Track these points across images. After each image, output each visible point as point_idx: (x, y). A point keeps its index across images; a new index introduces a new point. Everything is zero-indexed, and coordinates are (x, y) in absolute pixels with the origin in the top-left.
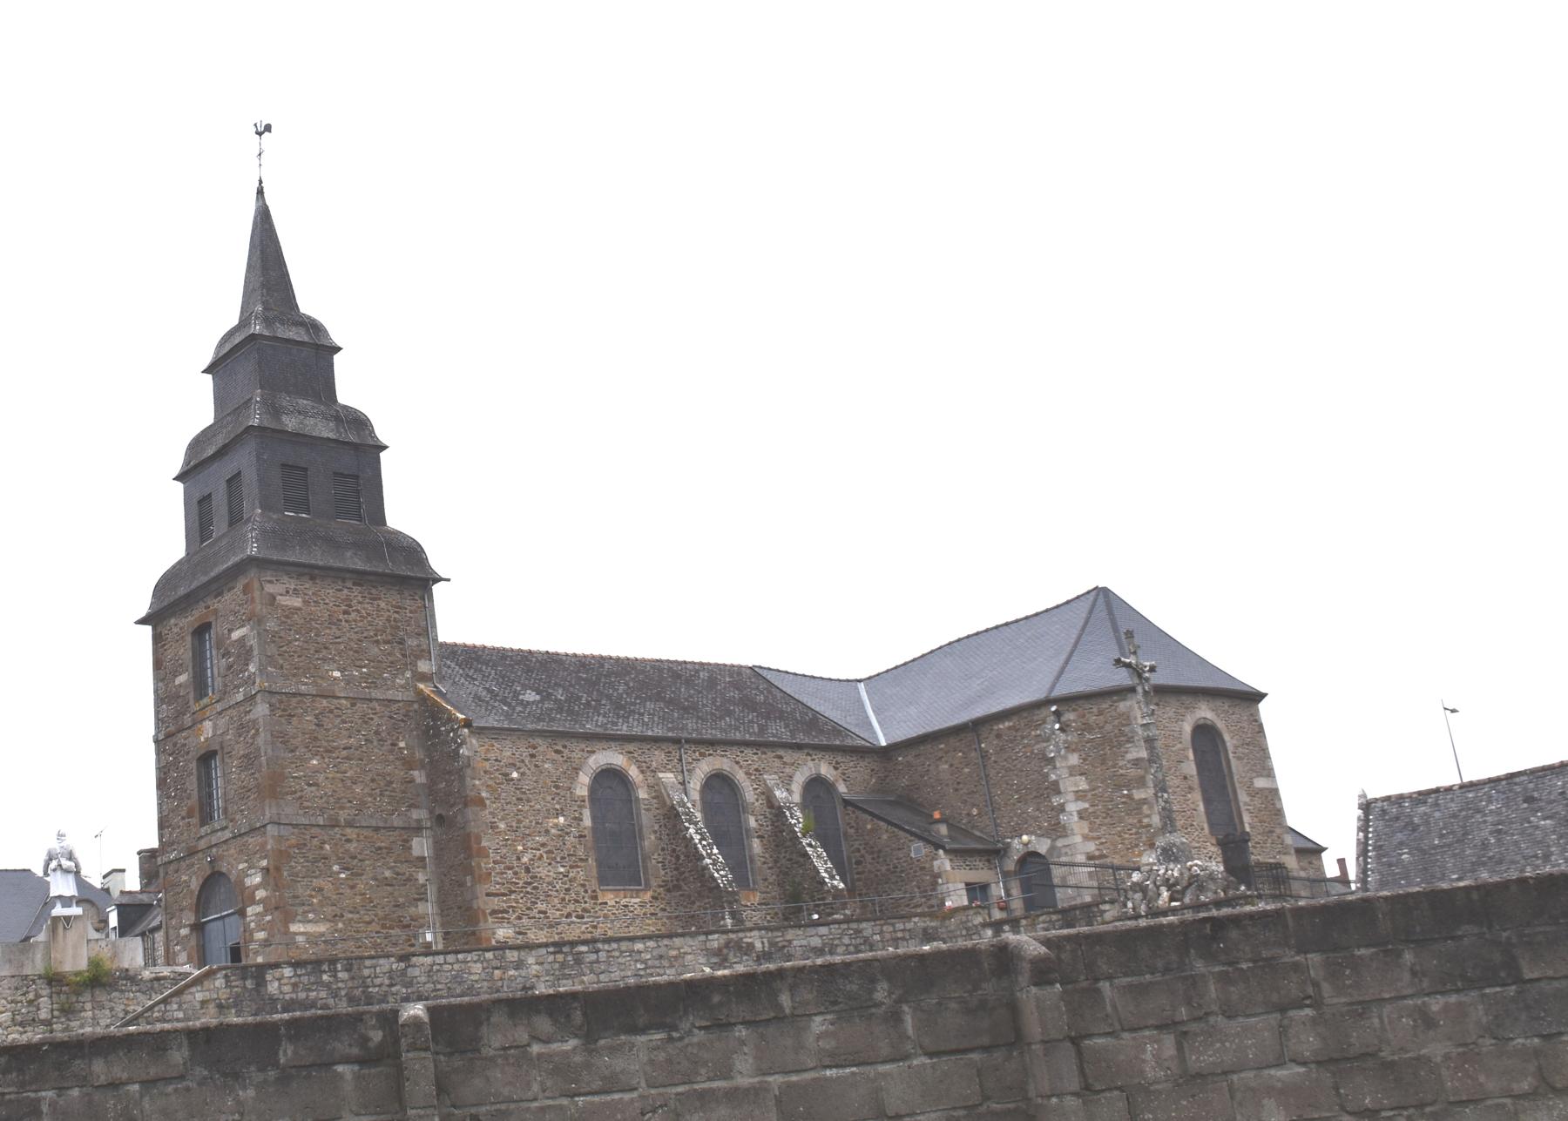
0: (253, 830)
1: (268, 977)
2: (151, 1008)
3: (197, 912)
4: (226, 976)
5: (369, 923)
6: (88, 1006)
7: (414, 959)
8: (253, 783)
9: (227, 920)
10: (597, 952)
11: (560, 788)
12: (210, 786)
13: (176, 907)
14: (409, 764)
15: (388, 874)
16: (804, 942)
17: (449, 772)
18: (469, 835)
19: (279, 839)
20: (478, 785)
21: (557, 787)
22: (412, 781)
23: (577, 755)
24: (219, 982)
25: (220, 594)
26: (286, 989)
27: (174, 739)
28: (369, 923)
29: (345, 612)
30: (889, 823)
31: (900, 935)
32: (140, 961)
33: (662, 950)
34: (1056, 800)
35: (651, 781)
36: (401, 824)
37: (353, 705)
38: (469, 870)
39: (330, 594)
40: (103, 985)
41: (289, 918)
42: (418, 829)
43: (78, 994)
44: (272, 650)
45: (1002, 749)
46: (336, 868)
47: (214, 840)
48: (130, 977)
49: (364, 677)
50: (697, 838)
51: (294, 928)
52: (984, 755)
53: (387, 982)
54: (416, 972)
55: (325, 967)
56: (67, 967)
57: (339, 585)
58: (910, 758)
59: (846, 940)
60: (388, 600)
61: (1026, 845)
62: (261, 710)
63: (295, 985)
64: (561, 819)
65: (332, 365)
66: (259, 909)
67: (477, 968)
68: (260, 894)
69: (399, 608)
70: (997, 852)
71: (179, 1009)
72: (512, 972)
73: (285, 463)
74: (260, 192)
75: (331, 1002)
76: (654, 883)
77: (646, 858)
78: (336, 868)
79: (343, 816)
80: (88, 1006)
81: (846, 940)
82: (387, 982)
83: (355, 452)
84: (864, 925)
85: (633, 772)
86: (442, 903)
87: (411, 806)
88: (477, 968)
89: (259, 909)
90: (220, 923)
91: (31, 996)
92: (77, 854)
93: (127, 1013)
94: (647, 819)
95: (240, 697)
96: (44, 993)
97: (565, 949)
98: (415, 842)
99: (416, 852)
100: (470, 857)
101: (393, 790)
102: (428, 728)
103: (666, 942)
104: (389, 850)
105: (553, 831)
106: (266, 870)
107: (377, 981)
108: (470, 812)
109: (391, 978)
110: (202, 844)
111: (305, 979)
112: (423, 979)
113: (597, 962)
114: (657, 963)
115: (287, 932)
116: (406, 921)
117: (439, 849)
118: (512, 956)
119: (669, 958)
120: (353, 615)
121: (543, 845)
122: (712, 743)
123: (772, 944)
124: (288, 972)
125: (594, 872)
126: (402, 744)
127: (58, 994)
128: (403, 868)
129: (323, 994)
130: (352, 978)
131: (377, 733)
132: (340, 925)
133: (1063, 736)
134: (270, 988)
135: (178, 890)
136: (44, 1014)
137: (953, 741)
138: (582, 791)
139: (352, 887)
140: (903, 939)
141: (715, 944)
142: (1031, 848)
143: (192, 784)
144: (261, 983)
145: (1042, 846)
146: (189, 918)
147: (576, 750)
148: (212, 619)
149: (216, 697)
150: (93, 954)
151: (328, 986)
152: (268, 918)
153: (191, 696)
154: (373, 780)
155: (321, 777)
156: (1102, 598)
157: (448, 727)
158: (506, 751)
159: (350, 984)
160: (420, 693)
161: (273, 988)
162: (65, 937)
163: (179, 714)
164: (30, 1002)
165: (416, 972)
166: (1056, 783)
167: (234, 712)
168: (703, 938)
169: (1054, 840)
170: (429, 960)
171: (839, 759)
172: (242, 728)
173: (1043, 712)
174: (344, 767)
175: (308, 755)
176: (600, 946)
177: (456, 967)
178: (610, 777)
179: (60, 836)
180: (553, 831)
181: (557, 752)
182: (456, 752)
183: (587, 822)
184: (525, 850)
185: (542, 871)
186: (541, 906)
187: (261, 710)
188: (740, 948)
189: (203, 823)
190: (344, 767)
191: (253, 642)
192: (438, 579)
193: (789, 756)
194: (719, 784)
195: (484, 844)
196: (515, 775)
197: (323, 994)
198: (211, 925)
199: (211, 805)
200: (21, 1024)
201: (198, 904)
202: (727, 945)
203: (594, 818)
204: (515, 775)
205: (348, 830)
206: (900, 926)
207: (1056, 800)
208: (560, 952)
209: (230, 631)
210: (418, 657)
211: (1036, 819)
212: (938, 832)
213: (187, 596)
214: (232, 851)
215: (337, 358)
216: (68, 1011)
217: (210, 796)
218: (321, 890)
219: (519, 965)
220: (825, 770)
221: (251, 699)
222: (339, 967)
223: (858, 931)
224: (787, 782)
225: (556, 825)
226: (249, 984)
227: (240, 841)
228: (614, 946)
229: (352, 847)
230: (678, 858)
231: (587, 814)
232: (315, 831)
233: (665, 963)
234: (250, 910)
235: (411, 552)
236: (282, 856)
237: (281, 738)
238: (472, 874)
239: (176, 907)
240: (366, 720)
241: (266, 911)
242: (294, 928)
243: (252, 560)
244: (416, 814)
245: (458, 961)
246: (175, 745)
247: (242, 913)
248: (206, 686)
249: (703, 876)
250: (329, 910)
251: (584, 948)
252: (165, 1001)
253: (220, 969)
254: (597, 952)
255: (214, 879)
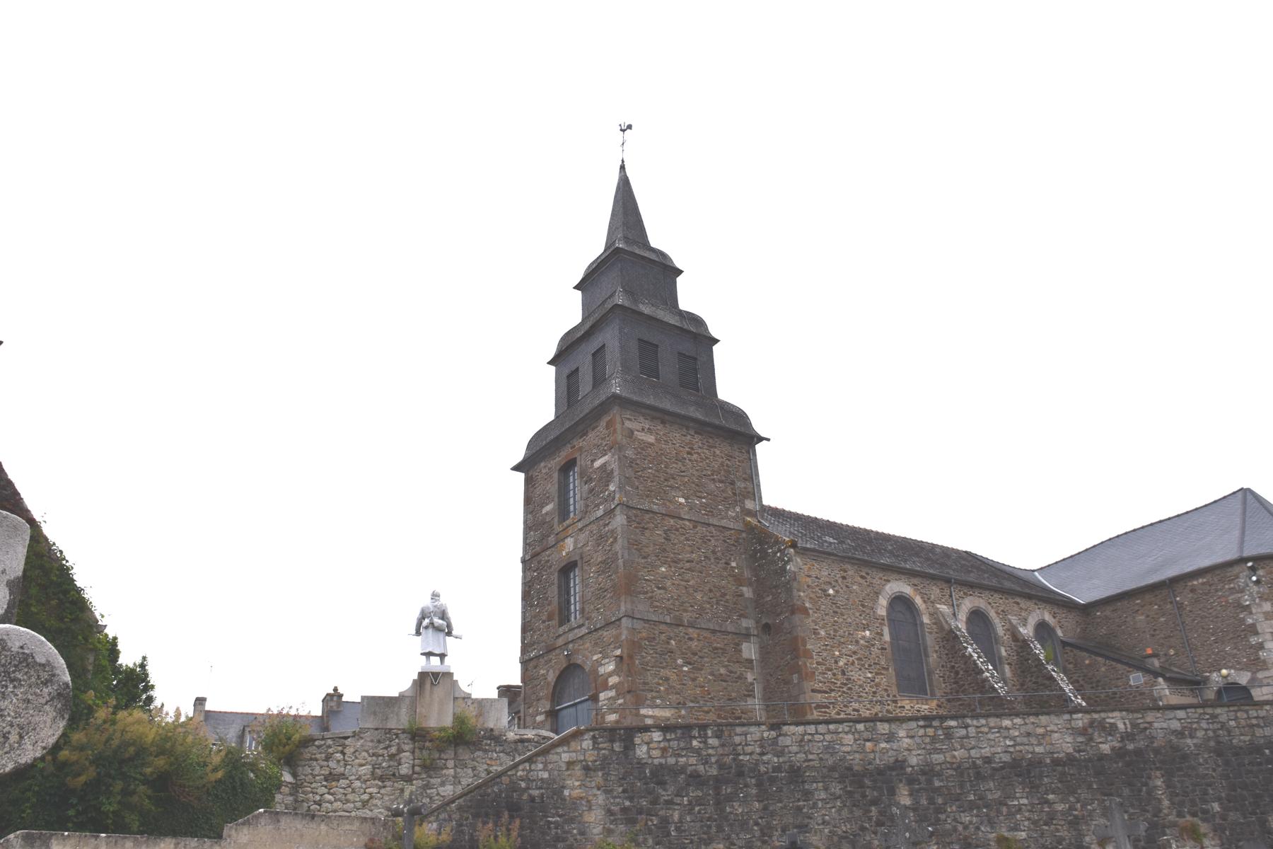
0: (608, 624)
1: (637, 740)
2: (515, 766)
3: (552, 701)
4: (594, 737)
5: (707, 712)
6: (451, 763)
7: (785, 728)
8: (609, 583)
9: (579, 707)
10: (966, 727)
11: (866, 606)
12: (568, 593)
13: (533, 697)
14: (739, 581)
15: (723, 671)
16: (1165, 725)
17: (776, 587)
18: (796, 638)
19: (633, 630)
20: (803, 596)
21: (863, 606)
22: (742, 595)
23: (877, 581)
24: (587, 743)
25: (586, 434)
26: (655, 753)
27: (539, 558)
28: (707, 712)
29: (689, 453)
30: (1107, 657)
31: (1254, 722)
32: (505, 719)
33: (1030, 728)
34: (1254, 640)
35: (931, 610)
36: (733, 630)
37: (695, 527)
38: (796, 669)
39: (677, 438)
40: (467, 744)
41: (639, 703)
42: (747, 636)
43: (441, 751)
44: (629, 473)
45: (1197, 601)
46: (680, 661)
47: (571, 636)
48: (495, 737)
49: (704, 506)
50: (975, 656)
51: (643, 711)
52: (1180, 606)
53: (758, 750)
54: (788, 741)
55: (695, 733)
56: (432, 723)
57: (684, 431)
58: (1108, 613)
59: (1204, 725)
60: (721, 450)
61: (1225, 677)
62: (619, 520)
63: (664, 750)
64: (868, 633)
65: (675, 283)
66: (612, 693)
67: (849, 739)
68: (613, 680)
69: (730, 457)
70: (1198, 683)
71: (544, 769)
72: (883, 745)
73: (636, 348)
74: (622, 168)
75: (701, 768)
76: (938, 693)
77: (930, 673)
78: (680, 661)
79: (686, 617)
80: (451, 763)
81: (1204, 725)
82: (758, 750)
83: (696, 341)
84: (1218, 711)
85: (918, 600)
86: (768, 696)
87: (741, 616)
88: (849, 739)
89: (612, 693)
90: (572, 710)
91: (393, 750)
92: (452, 614)
93: (489, 772)
94: (930, 640)
95: (600, 513)
96: (406, 747)
97: (936, 723)
98: (744, 646)
99: (745, 654)
100: (797, 657)
101: (727, 601)
102: (755, 551)
103: (1032, 719)
104: (724, 651)
105: (862, 642)
106: (620, 658)
107: (748, 749)
108: (797, 618)
109: (762, 746)
110: (560, 642)
111: (674, 744)
112: (795, 749)
113: (967, 737)
114: (1025, 740)
115: (638, 715)
116: (738, 713)
117: (764, 652)
118: (883, 728)
119: (1037, 736)
120: (695, 456)
121: (855, 653)
122: (972, 586)
123: (1134, 725)
124: (657, 736)
125: (894, 680)
126: (734, 564)
127: (421, 749)
128: (738, 669)
129: (693, 761)
130: (723, 745)
131: (714, 552)
132: (683, 712)
133: (1255, 588)
134: (638, 752)
135: (536, 682)
136: (404, 770)
137: (1148, 597)
138: (882, 612)
139: (694, 680)
140: (1258, 726)
141: (1080, 724)
142: (1230, 680)
143: (553, 592)
144: (629, 746)
145: (1243, 678)
146: (545, 706)
147: (876, 577)
148: (577, 455)
149: (578, 517)
150: (459, 710)
151: (697, 752)
152: (621, 701)
153: (556, 520)
154: (711, 591)
155: (669, 583)
156: (1246, 496)
157: (775, 549)
158: (824, 571)
159: (720, 751)
160: (747, 524)
161: (641, 751)
162: (431, 692)
163: (544, 537)
164: (392, 757)
165: (788, 741)
166: (1253, 625)
167: (594, 527)
168: (1067, 717)
169: (1254, 673)
170: (800, 729)
171: (1056, 610)
172: (601, 538)
173: (1236, 569)
174: (687, 576)
175: (658, 563)
176: (969, 721)
177: (828, 737)
178: (900, 601)
179: (435, 596)
180: (862, 642)
181: (862, 577)
182: (783, 569)
183: (887, 637)
184: (841, 655)
185: (855, 675)
186: (856, 705)
187: (619, 520)
188: (1104, 728)
189: (561, 624)
190: (687, 576)
191: (614, 466)
192: (761, 439)
193: (1024, 603)
194: (977, 617)
195: (809, 647)
196: (831, 591)
197: (693, 761)
198: (565, 712)
199: (569, 609)
200: (381, 778)
201: (553, 694)
202: (1092, 723)
203: (891, 634)
204: (831, 591)
205: (691, 630)
206: (1253, 713)
207: (1254, 640)
208: (930, 726)
209: (593, 461)
210: (745, 497)
211: (1234, 656)
212: (1153, 664)
213: (557, 438)
214: (588, 645)
215: (679, 280)
216: (430, 768)
217: (569, 602)
218: (667, 679)
219: (891, 737)
220: (1048, 617)
221: (610, 513)
222: (709, 733)
223: (1214, 716)
224: (1024, 622)
225: (864, 637)
226: (617, 747)
227: (595, 635)
228: (983, 721)
229: (694, 644)
230: (957, 673)
231: (886, 630)
232: (663, 627)
233: (1033, 740)
234: (602, 696)
235: (739, 417)
236: (635, 646)
237: (634, 544)
238: (799, 672)
239: (533, 697)
240: (705, 540)
241: (618, 696)
242: (643, 711)
243: (615, 397)
244: (745, 623)
245: (829, 732)
246: (539, 562)
247: (595, 698)
248: (569, 512)
249: (983, 686)
250: (673, 697)
251: (953, 723)
252: (530, 760)
253: (587, 730)
254: (966, 727)
255: (570, 670)
